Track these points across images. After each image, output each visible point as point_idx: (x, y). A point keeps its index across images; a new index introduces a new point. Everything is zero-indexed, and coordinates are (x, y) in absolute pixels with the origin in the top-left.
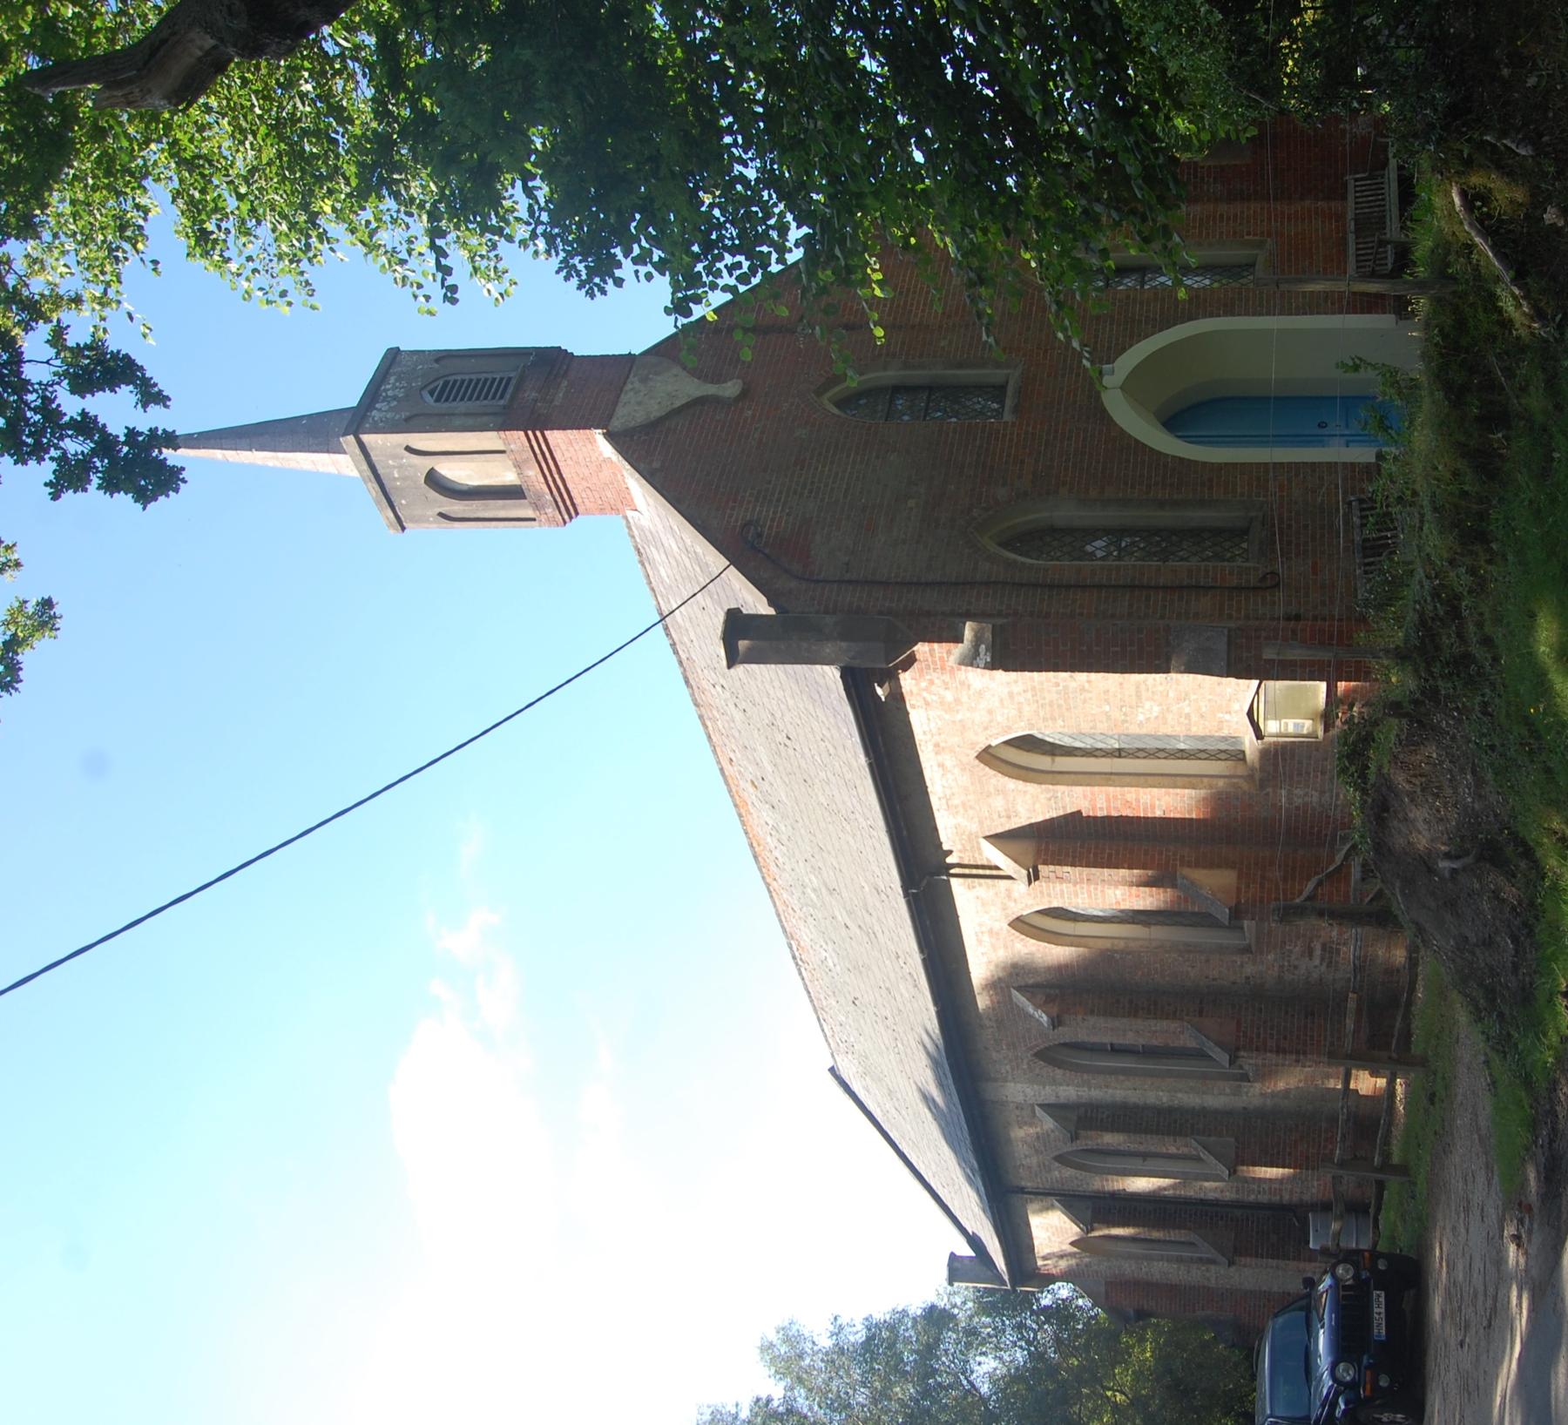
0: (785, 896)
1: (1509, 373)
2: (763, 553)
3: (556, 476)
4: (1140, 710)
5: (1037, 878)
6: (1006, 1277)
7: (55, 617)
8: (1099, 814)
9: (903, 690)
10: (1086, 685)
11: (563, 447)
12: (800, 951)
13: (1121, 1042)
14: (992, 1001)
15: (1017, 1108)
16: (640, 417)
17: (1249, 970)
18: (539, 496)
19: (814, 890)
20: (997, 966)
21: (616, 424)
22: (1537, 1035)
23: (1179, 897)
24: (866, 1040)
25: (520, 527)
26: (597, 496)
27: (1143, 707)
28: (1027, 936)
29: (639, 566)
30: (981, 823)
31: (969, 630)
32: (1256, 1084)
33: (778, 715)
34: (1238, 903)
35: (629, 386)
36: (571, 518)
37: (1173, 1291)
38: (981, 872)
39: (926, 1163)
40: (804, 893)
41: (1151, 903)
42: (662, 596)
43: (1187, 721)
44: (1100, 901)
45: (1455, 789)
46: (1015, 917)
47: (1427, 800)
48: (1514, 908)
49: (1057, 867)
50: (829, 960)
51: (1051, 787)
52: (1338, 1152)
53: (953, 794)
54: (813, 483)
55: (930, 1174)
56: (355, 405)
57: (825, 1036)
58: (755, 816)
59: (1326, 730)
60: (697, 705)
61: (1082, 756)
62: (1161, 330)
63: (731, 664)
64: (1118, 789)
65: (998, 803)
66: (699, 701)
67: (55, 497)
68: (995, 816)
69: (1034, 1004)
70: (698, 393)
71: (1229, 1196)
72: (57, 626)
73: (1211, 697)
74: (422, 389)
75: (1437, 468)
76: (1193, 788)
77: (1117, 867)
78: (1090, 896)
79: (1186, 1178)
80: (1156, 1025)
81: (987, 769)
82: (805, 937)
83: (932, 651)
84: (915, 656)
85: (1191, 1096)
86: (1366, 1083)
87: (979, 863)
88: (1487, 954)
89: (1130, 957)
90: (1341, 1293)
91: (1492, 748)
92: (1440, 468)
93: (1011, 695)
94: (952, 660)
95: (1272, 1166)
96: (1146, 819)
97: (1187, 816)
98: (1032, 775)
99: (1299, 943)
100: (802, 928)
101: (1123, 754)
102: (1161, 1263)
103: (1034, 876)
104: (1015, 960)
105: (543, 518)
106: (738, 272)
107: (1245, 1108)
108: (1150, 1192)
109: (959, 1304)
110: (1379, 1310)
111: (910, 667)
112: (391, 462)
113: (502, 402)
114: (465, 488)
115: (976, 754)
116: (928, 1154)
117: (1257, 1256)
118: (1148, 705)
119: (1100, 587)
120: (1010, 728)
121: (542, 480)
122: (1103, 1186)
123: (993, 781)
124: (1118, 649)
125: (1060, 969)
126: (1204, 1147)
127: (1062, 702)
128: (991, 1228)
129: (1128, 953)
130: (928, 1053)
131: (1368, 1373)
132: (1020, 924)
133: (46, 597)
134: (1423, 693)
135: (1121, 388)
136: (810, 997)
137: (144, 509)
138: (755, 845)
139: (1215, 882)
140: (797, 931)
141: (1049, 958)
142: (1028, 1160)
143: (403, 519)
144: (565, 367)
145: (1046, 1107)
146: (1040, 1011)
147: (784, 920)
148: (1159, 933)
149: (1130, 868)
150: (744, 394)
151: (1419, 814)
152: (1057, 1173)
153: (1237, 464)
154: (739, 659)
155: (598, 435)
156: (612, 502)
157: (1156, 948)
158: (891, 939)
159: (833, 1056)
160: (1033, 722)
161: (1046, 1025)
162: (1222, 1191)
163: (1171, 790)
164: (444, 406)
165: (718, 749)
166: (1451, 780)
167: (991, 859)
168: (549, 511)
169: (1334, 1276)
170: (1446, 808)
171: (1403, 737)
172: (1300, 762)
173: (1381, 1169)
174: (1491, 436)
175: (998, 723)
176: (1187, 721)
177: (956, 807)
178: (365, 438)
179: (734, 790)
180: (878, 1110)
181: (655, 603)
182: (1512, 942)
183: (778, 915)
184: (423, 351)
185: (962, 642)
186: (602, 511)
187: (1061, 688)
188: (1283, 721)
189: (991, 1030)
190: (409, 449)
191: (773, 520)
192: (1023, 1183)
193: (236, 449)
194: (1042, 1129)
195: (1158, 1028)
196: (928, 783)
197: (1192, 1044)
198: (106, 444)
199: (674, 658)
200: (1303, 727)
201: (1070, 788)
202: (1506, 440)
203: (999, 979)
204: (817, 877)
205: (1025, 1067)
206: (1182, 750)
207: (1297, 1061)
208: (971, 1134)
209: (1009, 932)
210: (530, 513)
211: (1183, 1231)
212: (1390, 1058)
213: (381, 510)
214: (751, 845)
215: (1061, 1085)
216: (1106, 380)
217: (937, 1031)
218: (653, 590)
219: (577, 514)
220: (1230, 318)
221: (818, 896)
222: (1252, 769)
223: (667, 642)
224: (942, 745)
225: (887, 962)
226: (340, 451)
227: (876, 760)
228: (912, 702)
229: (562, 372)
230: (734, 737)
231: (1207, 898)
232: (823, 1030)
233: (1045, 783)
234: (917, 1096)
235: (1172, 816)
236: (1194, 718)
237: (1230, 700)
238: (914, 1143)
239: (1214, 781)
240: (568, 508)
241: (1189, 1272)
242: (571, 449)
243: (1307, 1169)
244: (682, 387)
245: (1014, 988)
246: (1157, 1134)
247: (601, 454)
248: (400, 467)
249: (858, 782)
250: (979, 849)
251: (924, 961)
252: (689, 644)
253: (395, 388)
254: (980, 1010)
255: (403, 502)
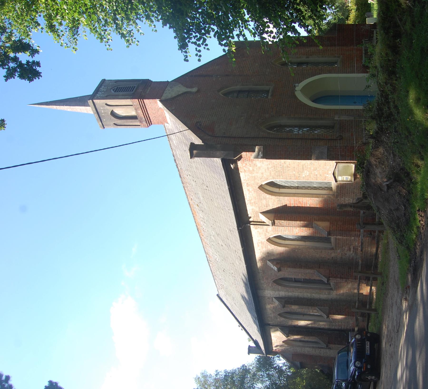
0: (206, 240)
1: (401, 20)
2: (201, 130)
3: (146, 113)
4: (303, 173)
5: (274, 224)
6: (264, 352)
7: (5, 124)
8: (292, 205)
9: (239, 167)
10: (289, 165)
11: (148, 105)
12: (209, 258)
13: (297, 277)
14: (261, 264)
15: (268, 298)
16: (169, 96)
17: (333, 255)
18: (141, 119)
19: (214, 236)
20: (263, 253)
21: (163, 98)
22: (411, 231)
23: (314, 232)
24: (227, 283)
25: (136, 128)
26: (157, 119)
27: (304, 172)
28: (271, 244)
29: (168, 141)
30: (259, 208)
31: (257, 149)
32: (335, 291)
33: (204, 180)
34: (330, 231)
35: (167, 89)
36: (150, 125)
37: (311, 357)
38: (259, 223)
39: (243, 319)
40: (211, 238)
41: (306, 234)
42: (174, 150)
43: (316, 177)
44: (292, 233)
45: (388, 161)
46: (268, 238)
47: (380, 166)
48: (404, 197)
49: (280, 221)
50: (217, 259)
51: (279, 197)
52: (357, 304)
53: (252, 199)
54: (216, 113)
55: (244, 323)
56: (92, 94)
57: (216, 284)
58: (198, 216)
59: (354, 180)
60: (183, 183)
61: (287, 189)
62: (312, 77)
63: (191, 157)
64: (297, 198)
65: (264, 202)
66: (183, 182)
67: (6, 80)
68: (263, 206)
69: (273, 264)
70: (186, 91)
71: (327, 327)
72: (5, 126)
73: (323, 169)
74: (111, 89)
75: (382, 54)
76: (318, 198)
77: (296, 221)
78: (289, 231)
79: (315, 321)
80: (307, 271)
81: (261, 191)
82: (211, 253)
83: (246, 154)
84: (242, 156)
85: (316, 295)
86: (365, 290)
87: (259, 221)
88: (397, 213)
89: (300, 251)
90: (357, 345)
91: (398, 142)
92: (382, 53)
93: (268, 168)
94: (252, 158)
95: (339, 315)
96: (305, 207)
97: (316, 206)
98: (273, 193)
99: (347, 246)
100: (210, 250)
101: (299, 188)
102: (308, 348)
103: (274, 224)
104: (268, 251)
105: (142, 125)
106: (197, 38)
107: (331, 299)
108: (305, 326)
109: (251, 369)
110: (368, 346)
111: (240, 160)
112: (101, 108)
113: (132, 92)
114: (121, 116)
115: (258, 187)
116: (244, 316)
117: (334, 344)
118: (305, 172)
119: (293, 139)
120: (267, 178)
121: (143, 114)
122: (292, 323)
123: (263, 195)
124: (298, 153)
125: (281, 254)
126: (320, 310)
127: (282, 171)
128: (260, 336)
129: (300, 250)
130: (244, 282)
131: (365, 364)
132: (270, 240)
133: (3, 119)
134: (379, 129)
135: (300, 91)
136: (212, 272)
137: (30, 82)
138: (198, 226)
139: (324, 225)
140: (209, 251)
141: (278, 251)
142: (271, 315)
143: (104, 125)
144: (150, 84)
145: (276, 298)
146: (275, 266)
147: (205, 249)
148: (308, 244)
149: (300, 221)
150: (198, 91)
151: (378, 171)
152: (279, 319)
153: (331, 109)
154: (193, 156)
155: (158, 101)
156: (161, 121)
157: (307, 248)
158: (234, 246)
159: (218, 291)
160: (274, 177)
161: (276, 271)
162: (325, 325)
163: (312, 198)
164: (117, 93)
165: (188, 196)
166: (387, 159)
167: (262, 219)
168: (144, 123)
169: (355, 338)
170: (385, 167)
171: (373, 146)
172: (347, 190)
173: (369, 310)
174: (396, 41)
175: (264, 177)
176: (316, 177)
177: (252, 203)
178: (95, 101)
179: (192, 209)
180: (230, 306)
181: (172, 152)
182: (404, 207)
183: (204, 247)
184: (112, 80)
185: (255, 152)
186: (158, 123)
187: (282, 166)
188: (343, 177)
189: (261, 273)
190: (106, 104)
191: (204, 122)
192: (269, 323)
193: (60, 106)
194: (275, 305)
195: (307, 272)
196: (245, 196)
197: (318, 278)
198: (21, 65)
199: (177, 169)
200: (348, 178)
201: (284, 197)
202: (400, 42)
203: (264, 257)
204: (214, 231)
205: (270, 285)
206: (315, 187)
207: (346, 281)
208: (255, 306)
209: (266, 242)
210: (139, 124)
211: (314, 337)
212: (371, 273)
213: (98, 122)
214: (197, 226)
215: (280, 291)
216: (297, 89)
217: (246, 273)
218: (172, 148)
219: (152, 124)
220: (330, 74)
221: (214, 238)
222: (334, 192)
223: (175, 164)
224: (249, 184)
225: (233, 254)
226: (88, 106)
227: (231, 187)
228: (241, 170)
229: (149, 85)
230: (193, 191)
231: (321, 229)
232: (215, 283)
233: (277, 196)
234: (241, 297)
235: (312, 206)
236: (318, 176)
237: (328, 170)
238: (239, 314)
239: (324, 196)
240: (149, 123)
241: (315, 351)
242: (150, 105)
243: (349, 316)
244: (182, 89)
245: (268, 260)
246: (307, 306)
247: (159, 106)
248: (104, 110)
249: (226, 195)
250: (259, 216)
251: (243, 250)
252: (181, 164)
253: (103, 89)
254: (258, 268)
255: (104, 120)
